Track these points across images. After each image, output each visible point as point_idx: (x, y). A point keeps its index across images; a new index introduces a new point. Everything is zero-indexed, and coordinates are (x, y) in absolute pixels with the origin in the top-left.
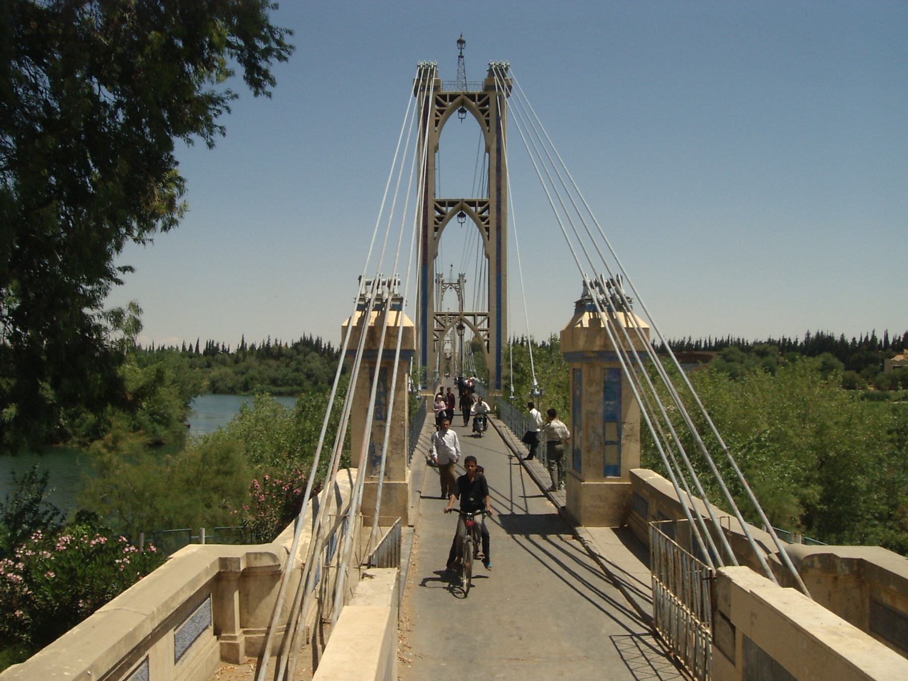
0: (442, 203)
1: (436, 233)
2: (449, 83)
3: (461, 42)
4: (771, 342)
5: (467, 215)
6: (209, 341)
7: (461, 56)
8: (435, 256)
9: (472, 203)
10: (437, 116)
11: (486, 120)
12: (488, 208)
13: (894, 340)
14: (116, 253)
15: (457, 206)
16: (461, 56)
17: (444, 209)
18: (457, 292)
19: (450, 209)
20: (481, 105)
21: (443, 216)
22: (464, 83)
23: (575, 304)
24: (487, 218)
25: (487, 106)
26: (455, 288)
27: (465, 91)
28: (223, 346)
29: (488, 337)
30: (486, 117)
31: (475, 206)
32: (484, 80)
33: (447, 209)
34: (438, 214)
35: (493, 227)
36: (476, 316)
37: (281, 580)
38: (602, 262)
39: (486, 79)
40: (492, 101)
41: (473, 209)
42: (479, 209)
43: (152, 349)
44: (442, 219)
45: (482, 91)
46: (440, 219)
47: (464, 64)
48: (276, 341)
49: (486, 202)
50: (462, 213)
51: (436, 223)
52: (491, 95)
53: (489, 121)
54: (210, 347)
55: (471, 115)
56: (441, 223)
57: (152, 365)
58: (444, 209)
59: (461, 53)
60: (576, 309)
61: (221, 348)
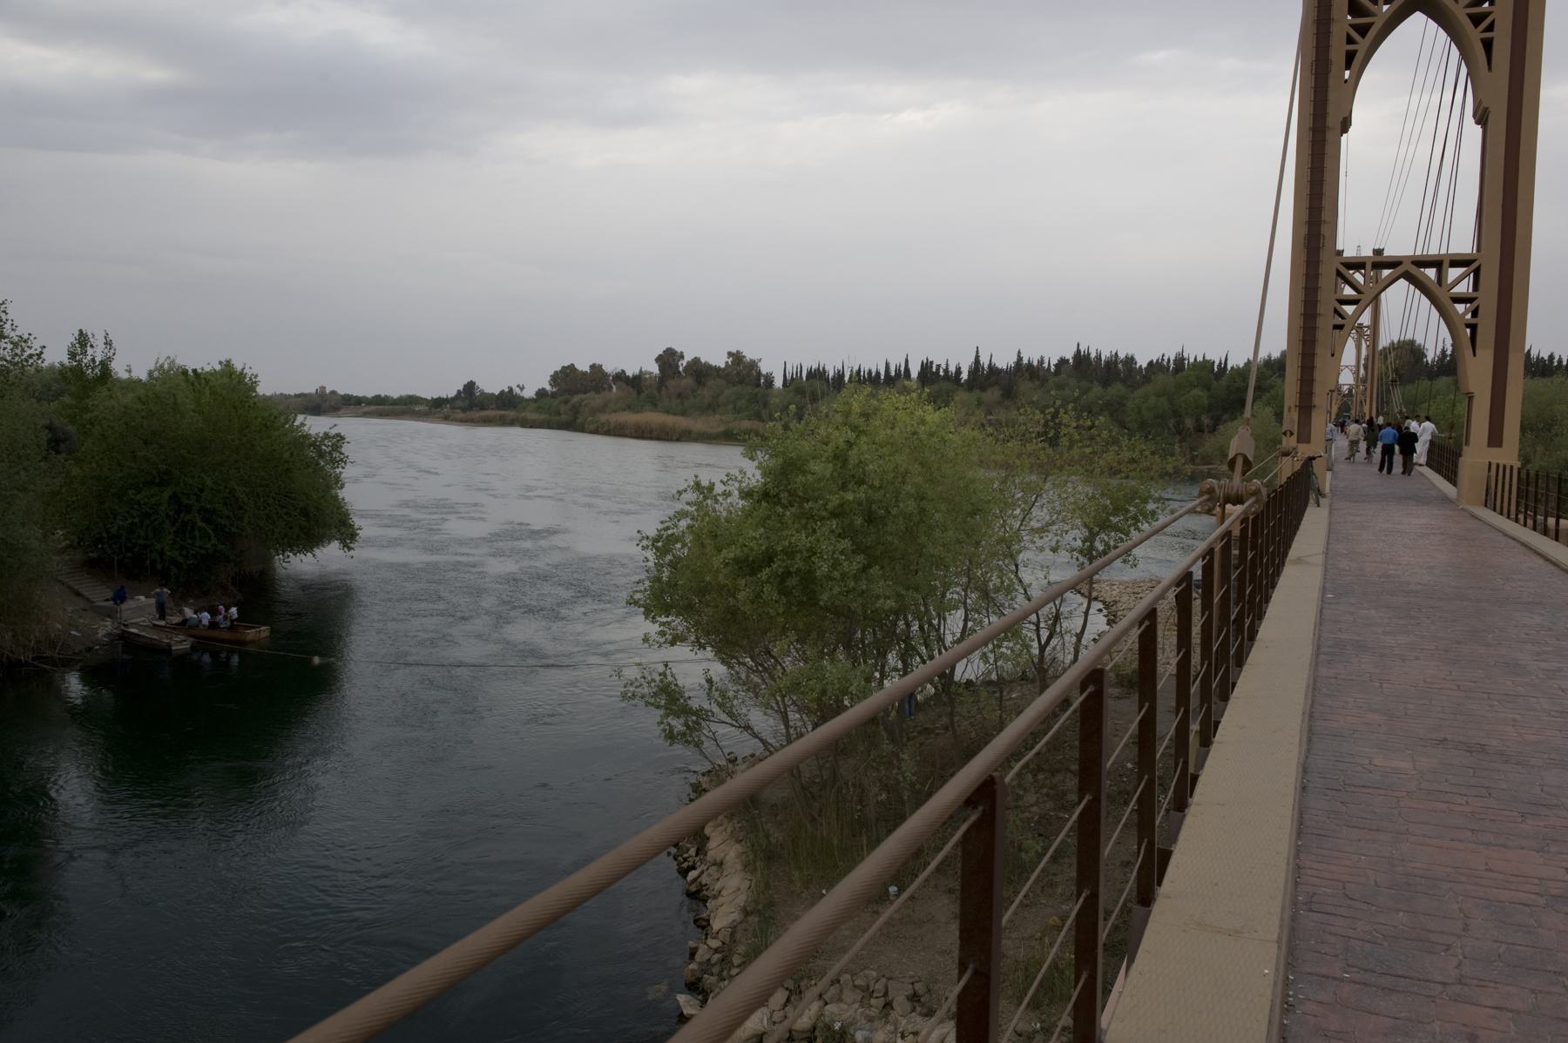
4: (364, 397)
6: (925, 361)
8: (1345, 125)
10: (1350, 41)
13: (1232, 368)
15: (1400, 270)
24: (1489, 14)
36: (1446, 264)
43: (794, 376)
48: (1163, 355)
49: (1474, 261)
51: (1350, 41)
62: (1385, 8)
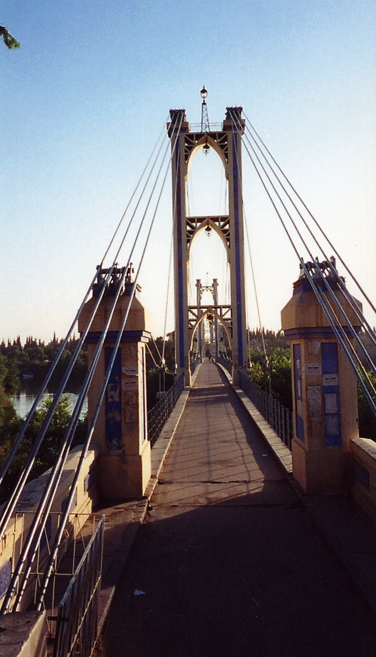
0: (192, 220)
2: (196, 125)
3: (204, 91)
5: (212, 228)
7: (204, 104)
9: (215, 219)
11: (225, 153)
16: (204, 104)
19: (199, 224)
20: (220, 142)
21: (193, 230)
22: (207, 124)
23: (293, 286)
25: (226, 143)
26: (211, 290)
27: (208, 131)
28: (40, 340)
29: (232, 325)
30: (224, 151)
31: (218, 221)
32: (222, 122)
33: (196, 224)
35: (232, 237)
37: (15, 542)
38: (289, 199)
39: (224, 121)
40: (230, 138)
41: (217, 223)
42: (222, 223)
45: (221, 131)
47: (206, 109)
49: (227, 218)
52: (230, 134)
53: (227, 153)
54: (29, 341)
55: (214, 150)
59: (204, 101)
60: (294, 290)
61: (38, 342)
62: (196, 141)
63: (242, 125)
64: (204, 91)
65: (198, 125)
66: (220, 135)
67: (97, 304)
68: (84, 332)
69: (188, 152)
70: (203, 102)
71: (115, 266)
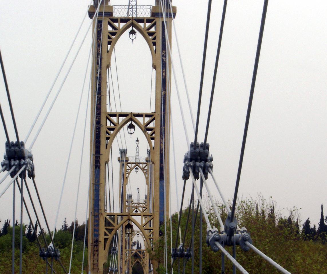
0: (114, 115)
1: (109, 46)
3: (137, 141)
7: (139, 192)
10: (109, 38)
12: (155, 24)
14: (227, 241)
17: (116, 24)
18: (145, 174)
21: (116, 31)
26: (143, 169)
28: (17, 221)
33: (119, 25)
34: (110, 29)
41: (141, 25)
44: (115, 34)
46: (113, 34)
50: (132, 30)
56: (114, 37)
57: (91, 245)
58: (116, 24)
63: (173, 13)
64: (138, 189)
65: (125, 7)
66: (149, 21)
67: (75, 233)
68: (75, 242)
69: (138, 251)
70: (136, 146)
71: (133, 245)
